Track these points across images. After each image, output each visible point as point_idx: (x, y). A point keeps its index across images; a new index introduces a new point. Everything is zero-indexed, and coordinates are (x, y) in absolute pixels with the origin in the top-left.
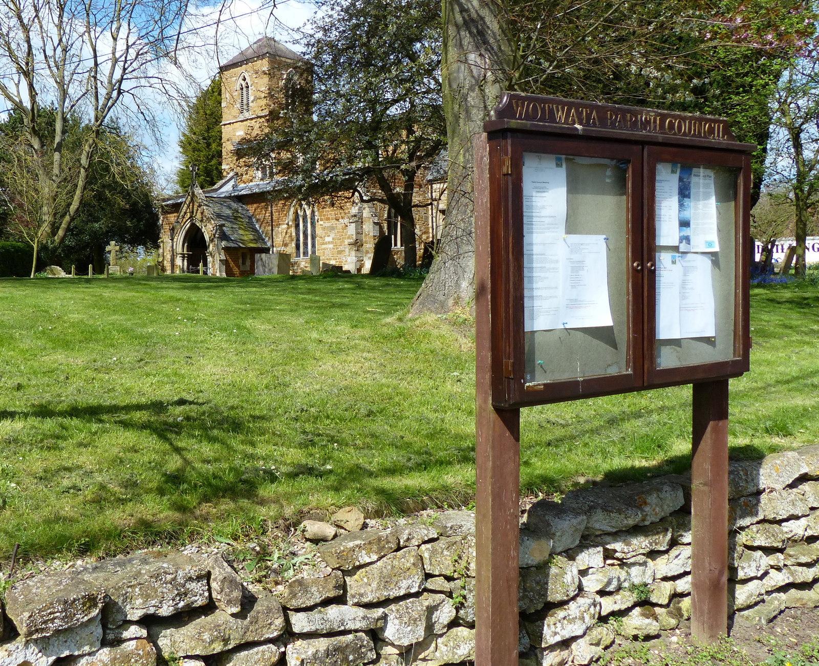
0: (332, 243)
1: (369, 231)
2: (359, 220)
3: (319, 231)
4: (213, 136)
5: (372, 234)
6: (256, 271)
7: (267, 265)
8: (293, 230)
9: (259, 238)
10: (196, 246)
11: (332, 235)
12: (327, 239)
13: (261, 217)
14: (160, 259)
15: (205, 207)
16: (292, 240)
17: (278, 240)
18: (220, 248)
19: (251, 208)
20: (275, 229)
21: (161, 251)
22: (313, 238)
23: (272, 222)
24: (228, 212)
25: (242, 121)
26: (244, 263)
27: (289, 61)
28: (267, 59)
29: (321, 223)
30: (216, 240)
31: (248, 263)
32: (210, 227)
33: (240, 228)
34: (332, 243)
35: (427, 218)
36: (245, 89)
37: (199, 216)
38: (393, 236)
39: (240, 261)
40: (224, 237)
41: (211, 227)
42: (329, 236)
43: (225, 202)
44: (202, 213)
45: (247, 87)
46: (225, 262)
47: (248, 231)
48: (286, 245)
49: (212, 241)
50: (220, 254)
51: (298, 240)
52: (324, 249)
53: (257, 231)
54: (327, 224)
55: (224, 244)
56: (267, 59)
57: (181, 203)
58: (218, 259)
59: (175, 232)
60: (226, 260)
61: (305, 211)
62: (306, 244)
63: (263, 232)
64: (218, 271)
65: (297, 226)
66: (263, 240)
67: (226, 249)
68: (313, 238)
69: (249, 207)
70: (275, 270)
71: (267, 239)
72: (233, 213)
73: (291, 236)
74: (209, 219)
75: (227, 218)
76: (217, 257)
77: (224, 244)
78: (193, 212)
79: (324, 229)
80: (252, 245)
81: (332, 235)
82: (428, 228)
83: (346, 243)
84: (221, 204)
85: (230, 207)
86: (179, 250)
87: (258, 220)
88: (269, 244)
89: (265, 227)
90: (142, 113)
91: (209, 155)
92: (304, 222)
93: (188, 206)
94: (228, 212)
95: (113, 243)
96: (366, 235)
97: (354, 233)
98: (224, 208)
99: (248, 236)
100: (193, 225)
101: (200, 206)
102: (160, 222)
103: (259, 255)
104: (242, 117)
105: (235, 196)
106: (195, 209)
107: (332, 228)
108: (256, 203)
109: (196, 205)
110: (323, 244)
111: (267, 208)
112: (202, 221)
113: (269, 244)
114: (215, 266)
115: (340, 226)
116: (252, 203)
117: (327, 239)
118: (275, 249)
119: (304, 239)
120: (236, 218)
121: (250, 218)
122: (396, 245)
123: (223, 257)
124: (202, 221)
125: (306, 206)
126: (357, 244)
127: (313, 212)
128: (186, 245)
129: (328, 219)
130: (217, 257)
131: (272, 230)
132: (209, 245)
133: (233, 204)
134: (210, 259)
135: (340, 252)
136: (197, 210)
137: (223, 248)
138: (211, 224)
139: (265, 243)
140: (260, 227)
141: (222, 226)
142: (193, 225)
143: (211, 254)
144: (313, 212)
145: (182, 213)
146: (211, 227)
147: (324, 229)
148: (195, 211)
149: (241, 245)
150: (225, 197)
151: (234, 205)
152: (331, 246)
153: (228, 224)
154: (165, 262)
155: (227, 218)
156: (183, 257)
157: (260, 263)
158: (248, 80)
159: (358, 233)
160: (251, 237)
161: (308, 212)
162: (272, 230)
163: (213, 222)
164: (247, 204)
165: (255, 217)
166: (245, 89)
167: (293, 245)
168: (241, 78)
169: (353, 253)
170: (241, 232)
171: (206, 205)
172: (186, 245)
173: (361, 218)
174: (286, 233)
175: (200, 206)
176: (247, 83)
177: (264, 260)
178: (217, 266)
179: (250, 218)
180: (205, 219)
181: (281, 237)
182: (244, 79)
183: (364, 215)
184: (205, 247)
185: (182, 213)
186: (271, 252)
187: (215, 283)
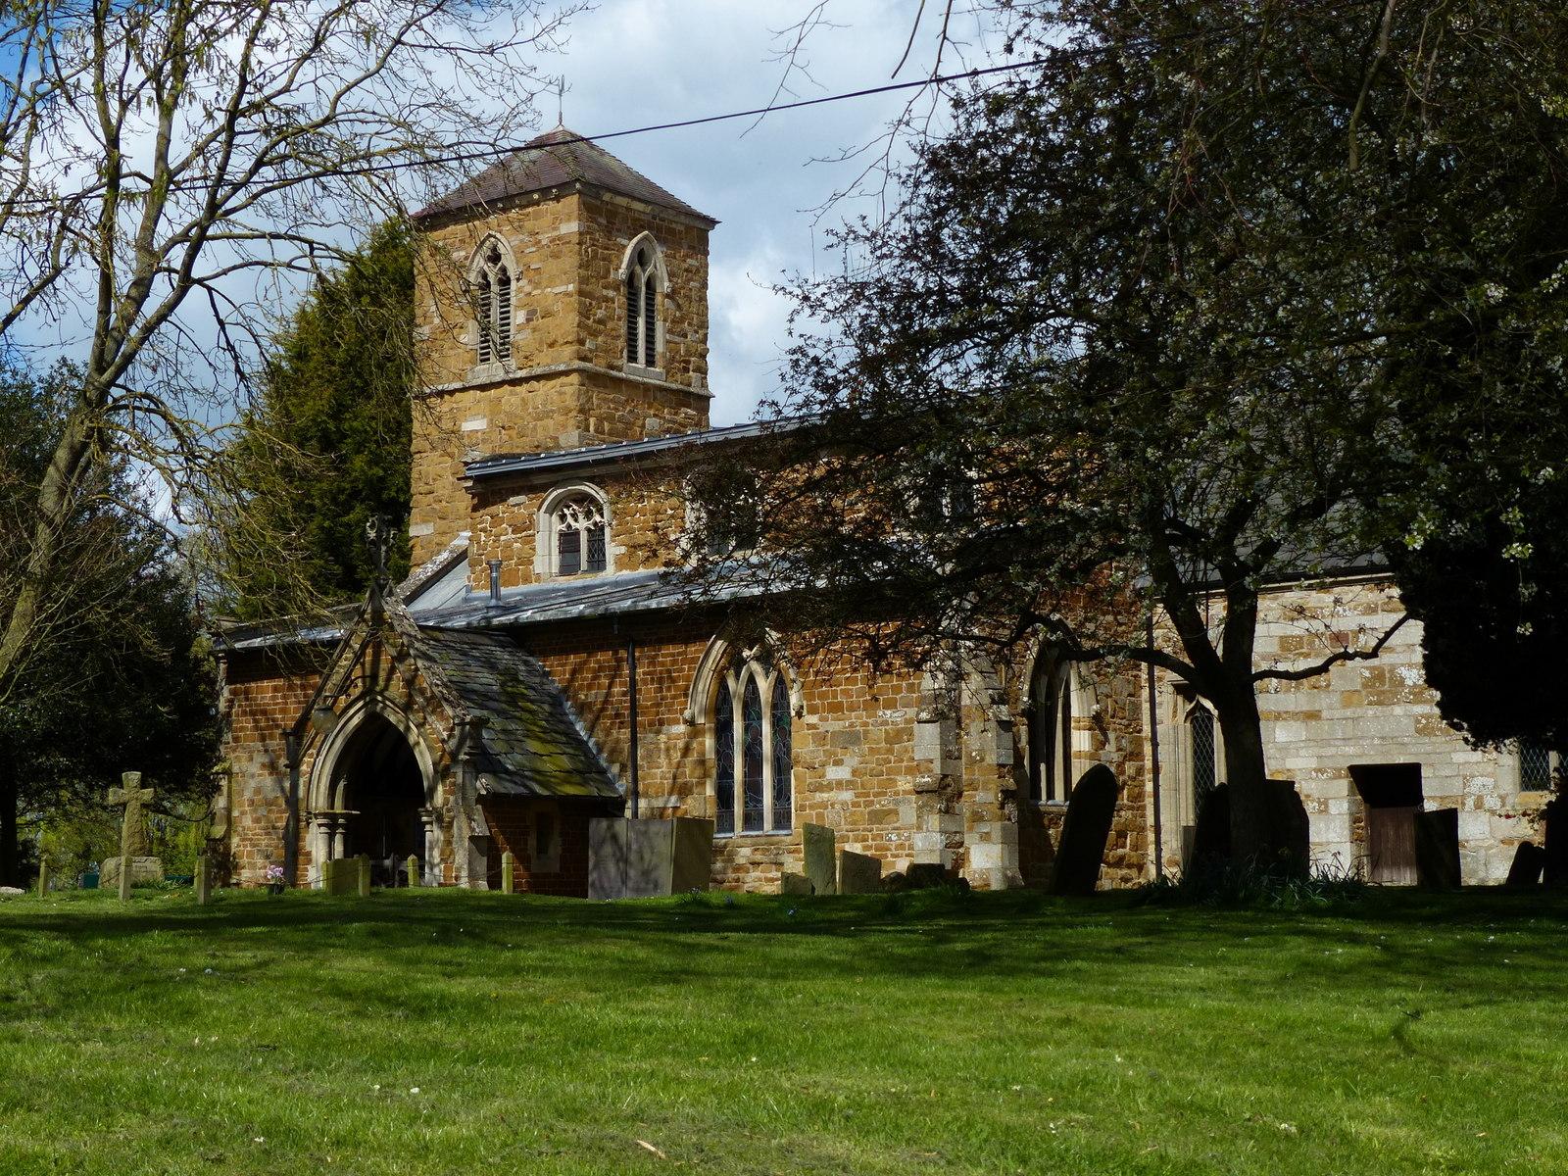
0: (849, 785)
1: (981, 751)
2: (947, 714)
3: (802, 745)
4: (354, 431)
5: (991, 759)
6: (592, 877)
7: (633, 857)
8: (709, 742)
9: (588, 767)
10: (381, 795)
11: (852, 761)
12: (833, 773)
13: (595, 696)
14: (219, 831)
15: (420, 663)
16: (706, 775)
17: (658, 772)
18: (472, 797)
19: (559, 670)
20: (646, 738)
21: (220, 802)
22: (782, 769)
23: (634, 713)
24: (486, 679)
25: (483, 388)
26: (542, 849)
27: (638, 206)
28: (576, 198)
29: (813, 719)
30: (459, 772)
31: (555, 848)
32: (439, 727)
33: (529, 734)
34: (849, 785)
35: (1137, 708)
36: (495, 288)
37: (397, 689)
38: (1043, 767)
39: (532, 842)
40: (483, 761)
41: (440, 726)
42: (838, 763)
43: (474, 646)
44: (410, 683)
45: (505, 282)
46: (485, 847)
47: (553, 742)
48: (683, 791)
49: (442, 773)
50: (470, 819)
51: (725, 774)
52: (824, 805)
53: (581, 744)
54: (834, 725)
55: (483, 784)
56: (576, 198)
57: (333, 643)
58: (466, 834)
59: (306, 741)
60: (490, 840)
61: (751, 680)
62: (753, 788)
63: (600, 748)
64: (464, 873)
65: (723, 730)
66: (603, 772)
67: (492, 804)
68: (782, 769)
69: (551, 664)
70: (666, 874)
71: (615, 769)
72: (503, 685)
73: (702, 762)
74: (434, 704)
75: (482, 698)
76: (462, 829)
77: (483, 784)
78: (374, 677)
79: (821, 739)
80: (570, 790)
81: (852, 761)
82: (1139, 743)
83: (904, 783)
84: (465, 654)
85: (491, 665)
86: (319, 800)
87: (582, 708)
88: (622, 786)
89: (608, 733)
90: (231, 348)
91: (341, 491)
92: (746, 716)
93: (359, 657)
94: (486, 679)
95: (133, 777)
96: (972, 762)
97: (935, 753)
98: (474, 667)
99: (556, 762)
100: (374, 723)
101: (402, 656)
102: (222, 705)
103: (604, 824)
104: (494, 370)
105: (503, 627)
106: (384, 666)
107: (851, 738)
108: (576, 651)
109: (389, 652)
110: (820, 788)
111: (618, 668)
112: (407, 708)
113: (622, 786)
114: (449, 860)
115: (879, 733)
116: (564, 651)
117: (833, 773)
118: (642, 803)
119: (750, 766)
120: (513, 699)
121: (556, 701)
122: (1051, 795)
123: (481, 829)
124: (407, 708)
125: (755, 666)
126: (945, 793)
127: (781, 688)
128: (341, 785)
129: (836, 708)
130: (462, 829)
131: (634, 741)
132: (433, 790)
133: (498, 652)
134: (433, 834)
135: (878, 817)
136: (392, 671)
137: (480, 799)
138: (443, 717)
139: (610, 784)
140: (591, 730)
141: (479, 724)
142: (374, 723)
143: (440, 819)
144: (781, 688)
145: (336, 679)
146: (440, 726)
147: (821, 739)
148: (382, 675)
149: (538, 789)
150: (469, 629)
151: (504, 657)
152: (847, 796)
153: (496, 722)
154: (235, 840)
155: (482, 698)
156: (332, 828)
157: (608, 849)
158: (508, 261)
159: (948, 756)
160: (565, 762)
161: (764, 685)
162: (634, 741)
163: (449, 711)
164: (544, 654)
165: (575, 698)
166: (495, 288)
167: (710, 791)
168: (486, 250)
169: (934, 821)
170: (533, 746)
171: (425, 656)
172: (341, 785)
173: (955, 705)
174: (686, 751)
175: (402, 656)
176: (504, 270)
177: (623, 839)
178: (461, 858)
179: (556, 701)
180: (420, 700)
181: (667, 769)
182: (495, 257)
183: (965, 701)
184: (414, 791)
185: (336, 679)
186: (628, 813)
187: (453, 923)
